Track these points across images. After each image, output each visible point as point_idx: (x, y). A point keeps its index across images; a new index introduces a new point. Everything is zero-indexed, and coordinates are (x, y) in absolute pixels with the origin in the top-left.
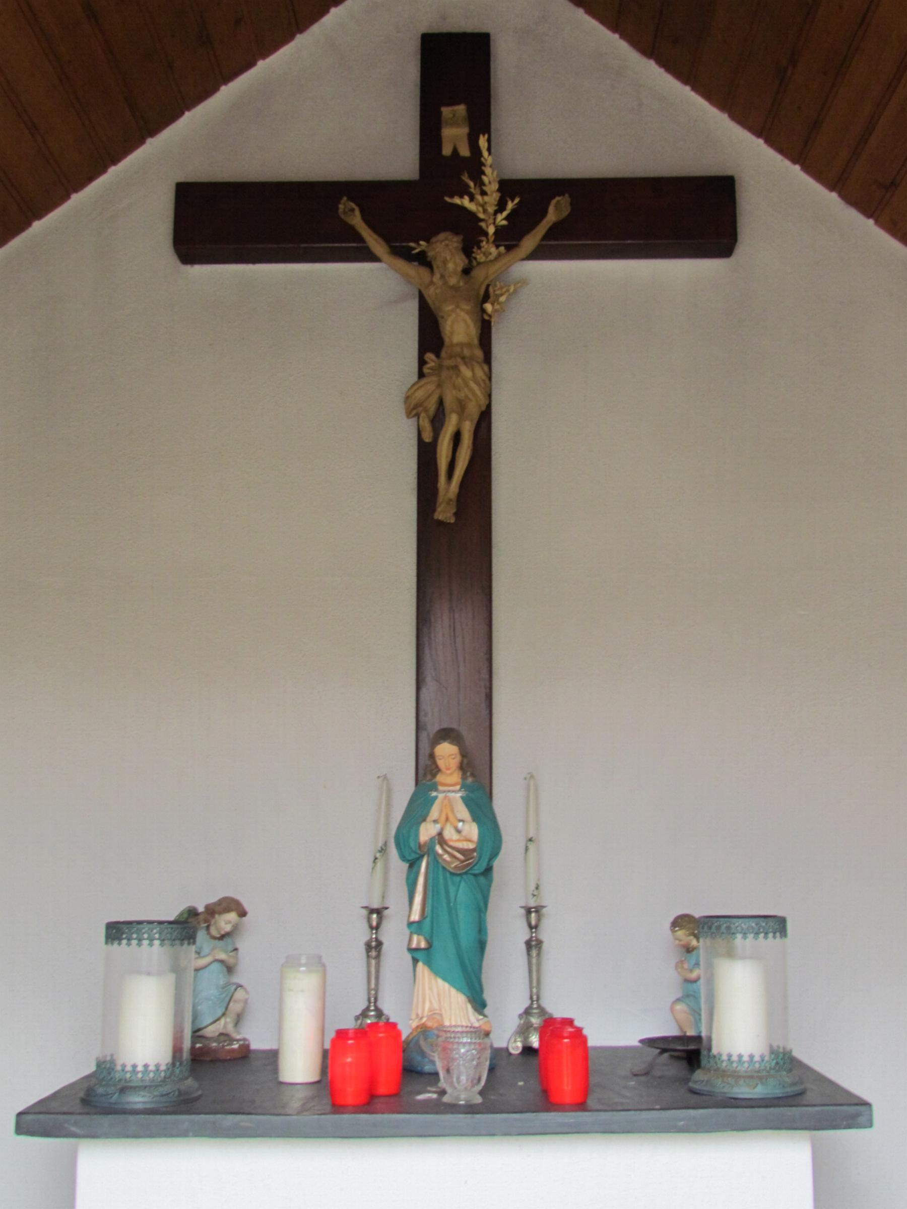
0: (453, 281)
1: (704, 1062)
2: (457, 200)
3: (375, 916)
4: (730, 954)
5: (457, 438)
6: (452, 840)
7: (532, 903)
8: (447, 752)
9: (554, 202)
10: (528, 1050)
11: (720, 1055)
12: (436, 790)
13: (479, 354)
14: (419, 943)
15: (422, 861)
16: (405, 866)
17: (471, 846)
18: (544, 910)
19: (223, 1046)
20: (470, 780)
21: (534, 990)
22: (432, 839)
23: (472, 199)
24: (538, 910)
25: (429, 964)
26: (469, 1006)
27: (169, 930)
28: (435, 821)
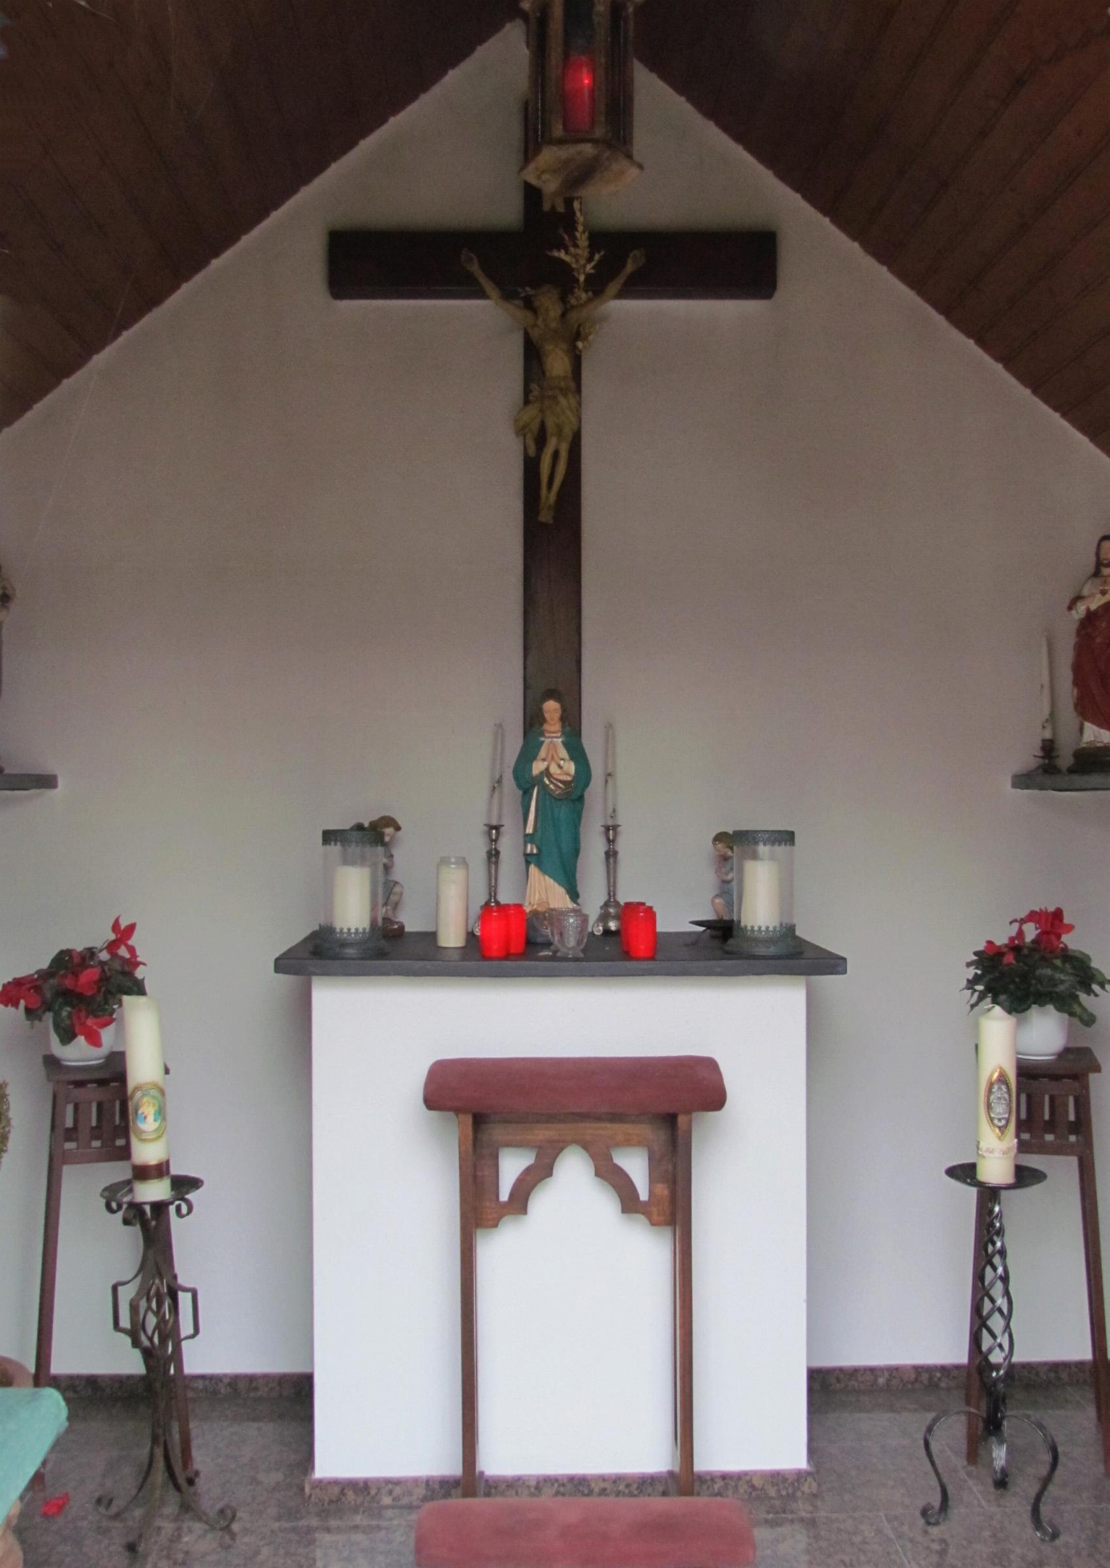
0: (553, 325)
1: (735, 933)
2: (556, 254)
3: (494, 831)
4: (755, 856)
5: (556, 455)
6: (555, 774)
7: (610, 823)
8: (551, 707)
9: (631, 255)
10: (607, 932)
11: (746, 927)
12: (544, 736)
13: (572, 385)
14: (532, 850)
15: (533, 790)
16: (521, 792)
17: (569, 779)
18: (619, 829)
19: (387, 926)
20: (568, 728)
21: (612, 889)
22: (541, 773)
23: (567, 253)
24: (615, 828)
25: (539, 865)
26: (568, 897)
27: (369, 836)
28: (544, 760)
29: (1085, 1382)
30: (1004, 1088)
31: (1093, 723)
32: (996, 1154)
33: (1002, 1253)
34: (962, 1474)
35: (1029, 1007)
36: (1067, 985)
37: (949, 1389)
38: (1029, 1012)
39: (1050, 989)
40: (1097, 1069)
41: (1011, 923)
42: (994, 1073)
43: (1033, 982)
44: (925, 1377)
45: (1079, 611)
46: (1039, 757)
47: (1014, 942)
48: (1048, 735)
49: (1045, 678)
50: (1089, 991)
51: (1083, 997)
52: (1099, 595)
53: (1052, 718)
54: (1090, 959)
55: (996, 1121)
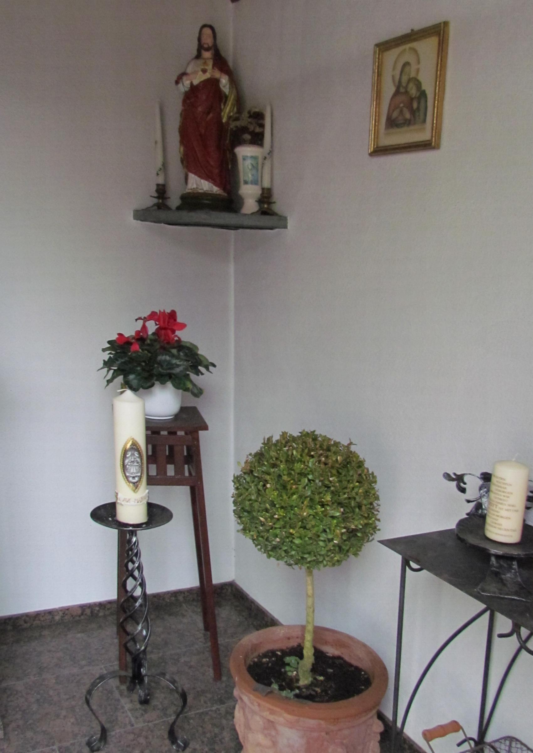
29: (194, 600)
30: (136, 454)
31: (195, 173)
32: (132, 503)
33: (140, 568)
34: (117, 695)
35: (152, 385)
36: (181, 368)
37: (105, 616)
38: (153, 389)
39: (168, 371)
40: (206, 428)
41: (136, 320)
42: (128, 443)
43: (156, 366)
44: (88, 611)
45: (185, 84)
46: (154, 197)
47: (140, 334)
48: (161, 181)
49: (158, 136)
50: (198, 373)
51: (193, 376)
52: (201, 73)
53: (165, 167)
54: (196, 347)
55: (131, 479)
